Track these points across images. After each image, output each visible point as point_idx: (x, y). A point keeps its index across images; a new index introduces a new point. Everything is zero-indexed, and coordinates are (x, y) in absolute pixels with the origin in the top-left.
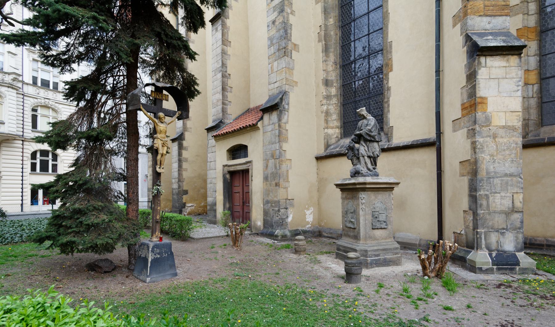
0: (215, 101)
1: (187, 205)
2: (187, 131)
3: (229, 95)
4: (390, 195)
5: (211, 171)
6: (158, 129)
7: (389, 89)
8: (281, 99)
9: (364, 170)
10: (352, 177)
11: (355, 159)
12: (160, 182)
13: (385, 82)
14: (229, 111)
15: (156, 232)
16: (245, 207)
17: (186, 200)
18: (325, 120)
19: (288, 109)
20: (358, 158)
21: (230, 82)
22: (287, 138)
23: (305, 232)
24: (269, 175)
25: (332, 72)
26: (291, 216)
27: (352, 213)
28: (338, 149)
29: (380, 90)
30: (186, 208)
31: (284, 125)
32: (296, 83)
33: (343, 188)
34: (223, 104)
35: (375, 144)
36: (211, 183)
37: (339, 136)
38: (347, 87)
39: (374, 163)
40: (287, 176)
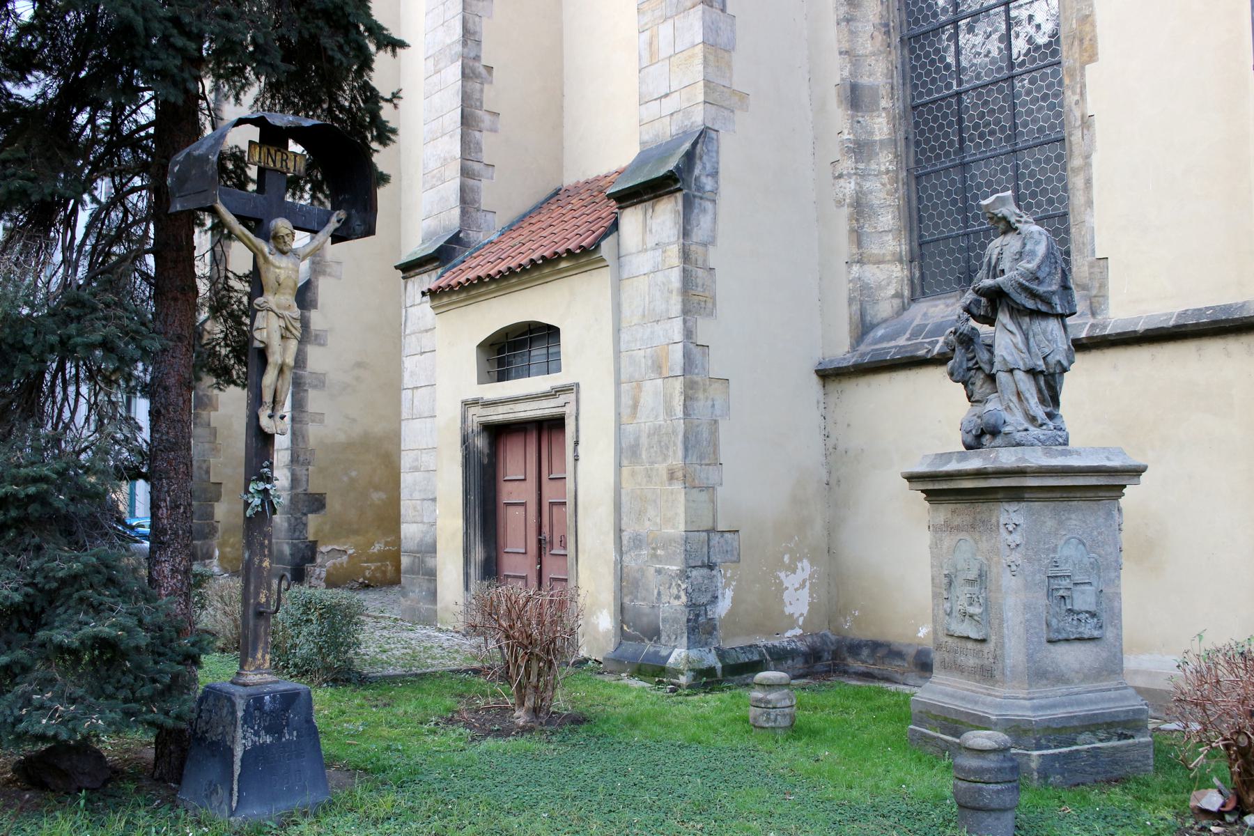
0: (432, 165)
1: (323, 549)
2: (324, 273)
3: (486, 140)
4: (1109, 514)
5: (417, 424)
6: (269, 277)
7: (1087, 122)
8: (690, 156)
9: (1015, 421)
10: (968, 447)
11: (979, 379)
12: (271, 466)
13: (1070, 98)
14: (485, 201)
15: (255, 650)
16: (547, 560)
17: (316, 533)
18: (852, 231)
19: (715, 191)
20: (992, 378)
21: (491, 96)
22: (714, 298)
23: (779, 657)
24: (644, 441)
25: (872, 60)
26: (729, 594)
27: (971, 582)
28: (902, 341)
29: (1052, 127)
30: (319, 560)
31: (700, 249)
32: (743, 97)
33: (939, 488)
34: (465, 172)
35: (1053, 325)
36: (416, 469)
37: (906, 293)
38: (930, 111)
39: (1051, 396)
40: (714, 445)
